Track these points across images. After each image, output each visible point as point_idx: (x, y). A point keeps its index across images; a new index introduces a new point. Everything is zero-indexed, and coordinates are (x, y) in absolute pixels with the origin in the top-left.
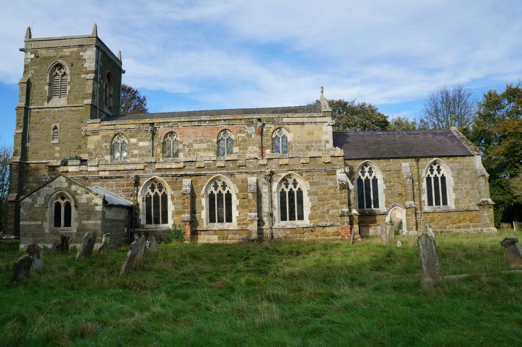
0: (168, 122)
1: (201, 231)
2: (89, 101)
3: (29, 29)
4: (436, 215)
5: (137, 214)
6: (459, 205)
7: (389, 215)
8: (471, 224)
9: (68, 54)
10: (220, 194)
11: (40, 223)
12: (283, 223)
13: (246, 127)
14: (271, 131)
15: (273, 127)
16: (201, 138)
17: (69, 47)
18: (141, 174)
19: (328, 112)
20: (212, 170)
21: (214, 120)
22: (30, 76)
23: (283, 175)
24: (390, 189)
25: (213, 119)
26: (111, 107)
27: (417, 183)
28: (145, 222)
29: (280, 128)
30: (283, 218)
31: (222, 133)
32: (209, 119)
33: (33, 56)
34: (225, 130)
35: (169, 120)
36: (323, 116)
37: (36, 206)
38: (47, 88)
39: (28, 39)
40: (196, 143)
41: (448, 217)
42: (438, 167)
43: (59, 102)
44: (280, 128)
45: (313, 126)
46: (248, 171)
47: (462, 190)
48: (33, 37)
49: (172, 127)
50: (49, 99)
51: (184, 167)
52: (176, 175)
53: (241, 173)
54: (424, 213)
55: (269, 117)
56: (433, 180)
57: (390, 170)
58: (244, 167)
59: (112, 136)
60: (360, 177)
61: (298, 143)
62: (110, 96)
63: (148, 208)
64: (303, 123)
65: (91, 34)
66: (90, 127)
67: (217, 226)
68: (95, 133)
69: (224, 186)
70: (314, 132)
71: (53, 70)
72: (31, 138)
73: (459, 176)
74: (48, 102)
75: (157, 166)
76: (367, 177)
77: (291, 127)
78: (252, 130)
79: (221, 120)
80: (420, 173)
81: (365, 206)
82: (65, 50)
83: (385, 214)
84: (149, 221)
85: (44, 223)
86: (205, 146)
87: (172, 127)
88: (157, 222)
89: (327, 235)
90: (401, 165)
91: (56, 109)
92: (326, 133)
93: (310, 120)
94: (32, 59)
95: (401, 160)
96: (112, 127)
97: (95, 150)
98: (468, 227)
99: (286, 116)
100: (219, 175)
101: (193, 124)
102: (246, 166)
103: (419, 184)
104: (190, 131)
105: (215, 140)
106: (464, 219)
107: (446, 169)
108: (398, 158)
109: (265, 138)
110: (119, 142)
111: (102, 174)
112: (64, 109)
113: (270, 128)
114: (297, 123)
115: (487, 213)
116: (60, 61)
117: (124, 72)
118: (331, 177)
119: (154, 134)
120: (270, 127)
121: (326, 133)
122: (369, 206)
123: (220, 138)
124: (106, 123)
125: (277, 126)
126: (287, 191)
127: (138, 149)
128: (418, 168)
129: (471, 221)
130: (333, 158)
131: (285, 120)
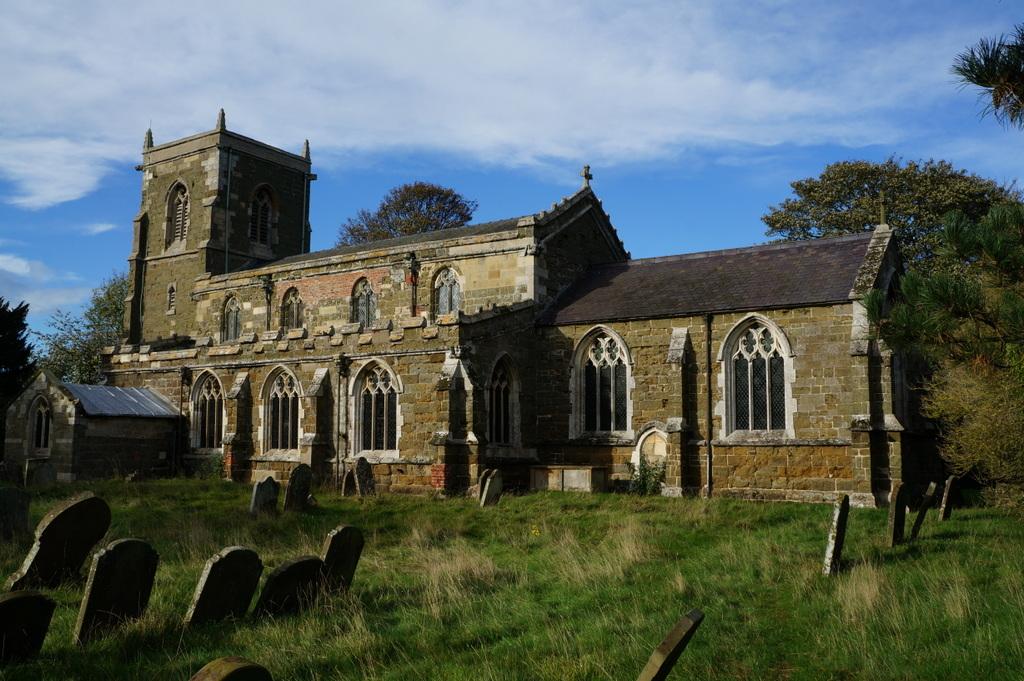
0: (289, 271)
1: (257, 461)
2: (204, 243)
3: (150, 134)
4: (746, 453)
5: (187, 431)
6: (805, 430)
7: (638, 447)
9: (189, 166)
11: (20, 441)
13: (392, 271)
14: (431, 275)
15: (434, 267)
16: (330, 296)
17: (188, 155)
19: (528, 226)
20: (273, 356)
21: (348, 262)
22: (147, 208)
23: (364, 363)
24: (644, 388)
25: (345, 259)
26: (275, 245)
27: (705, 375)
28: (199, 444)
29: (445, 268)
31: (360, 285)
32: (340, 260)
33: (151, 176)
34: (362, 279)
35: (289, 268)
36: (518, 237)
37: (19, 417)
38: (164, 225)
39: (146, 150)
40: (324, 306)
41: (776, 460)
43: (179, 246)
44: (445, 268)
45: (500, 258)
46: (316, 357)
47: (816, 390)
48: (157, 143)
49: (293, 279)
50: (168, 243)
51: (240, 352)
52: (229, 367)
54: (715, 446)
55: (427, 247)
57: (646, 344)
58: (312, 351)
59: (223, 299)
60: (590, 362)
61: (474, 296)
62: (274, 226)
64: (481, 255)
65: (215, 128)
66: (201, 286)
68: (204, 295)
69: (386, 379)
70: (502, 271)
71: (172, 196)
72: (146, 307)
74: (166, 248)
75: (212, 351)
76: (758, 353)
78: (400, 275)
79: (357, 261)
80: (712, 352)
81: (598, 425)
82: (186, 160)
83: (630, 445)
84: (203, 445)
85: (865, 417)
86: (333, 310)
87: (293, 279)
88: (211, 446)
91: (174, 259)
92: (523, 271)
93: (497, 246)
94: (150, 181)
95: (672, 321)
96: (223, 285)
97: (204, 324)
98: (828, 487)
99: (454, 243)
100: (280, 365)
102: (313, 348)
103: (709, 376)
104: (316, 283)
105: (348, 298)
107: (777, 337)
109: (420, 289)
110: (234, 309)
111: (156, 366)
112: (182, 258)
113: (429, 269)
114: (472, 256)
115: (861, 453)
116: (180, 180)
117: (314, 177)
118: (437, 366)
120: (428, 268)
121: (523, 271)
122: (606, 426)
123: (357, 294)
124: (217, 278)
125: (440, 265)
126: (373, 393)
127: (252, 320)
128: (709, 338)
130: (441, 328)
131: (453, 251)
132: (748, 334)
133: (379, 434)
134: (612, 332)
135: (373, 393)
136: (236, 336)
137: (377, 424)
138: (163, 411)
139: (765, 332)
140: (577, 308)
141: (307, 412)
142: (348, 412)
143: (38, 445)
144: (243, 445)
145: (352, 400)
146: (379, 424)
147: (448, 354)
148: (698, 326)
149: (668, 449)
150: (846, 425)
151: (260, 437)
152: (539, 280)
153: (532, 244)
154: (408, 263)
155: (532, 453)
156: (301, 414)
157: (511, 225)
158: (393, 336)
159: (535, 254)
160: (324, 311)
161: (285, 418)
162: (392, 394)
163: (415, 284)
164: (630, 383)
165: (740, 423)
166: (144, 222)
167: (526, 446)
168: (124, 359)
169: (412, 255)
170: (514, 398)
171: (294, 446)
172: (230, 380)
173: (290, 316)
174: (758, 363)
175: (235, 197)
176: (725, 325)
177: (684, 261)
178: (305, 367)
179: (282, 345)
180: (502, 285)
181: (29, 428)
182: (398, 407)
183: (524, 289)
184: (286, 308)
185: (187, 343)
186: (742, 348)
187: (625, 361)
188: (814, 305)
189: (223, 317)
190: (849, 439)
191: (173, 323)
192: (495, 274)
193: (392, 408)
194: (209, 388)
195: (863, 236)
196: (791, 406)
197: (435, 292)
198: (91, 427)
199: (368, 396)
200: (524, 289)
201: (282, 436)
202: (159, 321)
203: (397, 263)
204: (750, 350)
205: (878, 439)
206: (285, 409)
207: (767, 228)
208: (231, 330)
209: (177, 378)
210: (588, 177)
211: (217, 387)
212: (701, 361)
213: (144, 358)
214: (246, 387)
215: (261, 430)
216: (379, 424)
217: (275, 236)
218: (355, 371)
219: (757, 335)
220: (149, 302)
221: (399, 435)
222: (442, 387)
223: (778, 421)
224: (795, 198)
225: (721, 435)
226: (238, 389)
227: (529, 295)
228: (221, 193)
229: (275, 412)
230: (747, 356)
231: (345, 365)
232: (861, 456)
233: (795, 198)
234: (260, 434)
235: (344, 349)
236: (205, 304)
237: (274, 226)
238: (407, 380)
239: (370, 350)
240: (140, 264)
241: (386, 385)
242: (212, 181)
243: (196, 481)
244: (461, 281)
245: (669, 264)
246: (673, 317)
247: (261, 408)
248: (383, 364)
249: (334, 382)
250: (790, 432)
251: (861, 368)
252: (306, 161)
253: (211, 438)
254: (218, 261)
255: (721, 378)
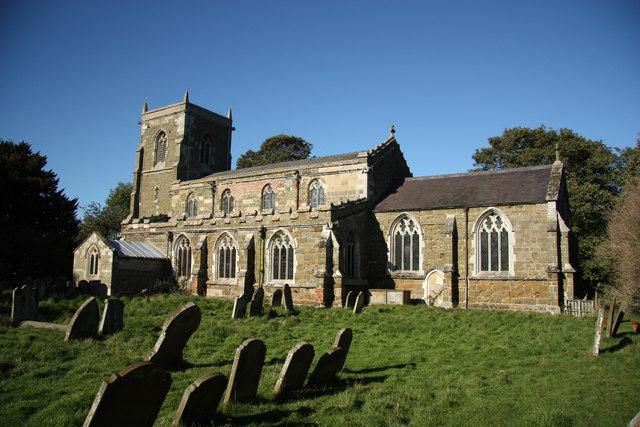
2: (176, 164)
4: (487, 283)
8: (537, 299)
10: (494, 233)
12: (274, 281)
17: (167, 116)
18: (174, 230)
23: (275, 231)
30: (276, 277)
42: (498, 218)
43: (161, 165)
45: (348, 174)
47: (527, 250)
50: (155, 164)
52: (196, 232)
53: (241, 229)
56: (411, 238)
62: (212, 155)
63: (398, 248)
64: (337, 172)
66: (175, 187)
67: (224, 280)
68: (177, 192)
69: (288, 241)
71: (159, 137)
73: (523, 229)
77: (326, 177)
78: (290, 183)
86: (251, 201)
89: (308, 296)
90: (445, 216)
101: (262, 178)
104: (241, 186)
105: (260, 195)
106: (528, 291)
107: (506, 220)
108: (443, 208)
110: (193, 200)
111: (152, 230)
114: (331, 173)
116: (163, 129)
117: (234, 129)
119: (214, 191)
120: (305, 180)
124: (184, 183)
126: (280, 248)
129: (537, 294)
131: (321, 170)
132: (402, 222)
133: (283, 271)
134: (411, 216)
135: (280, 248)
136: (195, 215)
137: (283, 262)
138: (159, 256)
139: (498, 218)
140: (391, 200)
141: (241, 258)
142: (267, 257)
143: (91, 273)
144: (203, 276)
145: (267, 252)
146: (283, 266)
147: (325, 227)
148: (459, 214)
149: (444, 281)
150: (543, 269)
151: (213, 271)
152: (370, 187)
153: (368, 168)
154: (295, 177)
155: (366, 282)
156: (237, 259)
157: (354, 156)
158: (292, 216)
159: (368, 173)
160: (245, 202)
161: (228, 261)
162: (291, 249)
163: (298, 189)
164: (422, 244)
165: (484, 267)
166: (142, 151)
167: (363, 278)
168: (135, 226)
169: (297, 172)
170: (357, 251)
171: (233, 276)
172: (196, 239)
173: (226, 204)
174: (407, 237)
175: (192, 139)
176: (476, 213)
177: (446, 180)
178: (240, 233)
179: (227, 220)
180: (350, 189)
181: (87, 263)
182: (295, 256)
183: (361, 192)
184: (223, 200)
185: (165, 218)
186: (485, 226)
187: (419, 233)
188: (525, 203)
189: (187, 205)
190: (546, 276)
191: (158, 207)
192: (345, 183)
193: (291, 256)
194: (183, 243)
195: (549, 166)
196: (512, 259)
197: (310, 193)
198: (121, 263)
199: (277, 250)
200: (361, 192)
201: (227, 270)
202: (148, 207)
203: (288, 176)
204: (489, 227)
205: (561, 277)
206: (185, 256)
207: (474, 162)
208: (192, 212)
209: (165, 237)
210: (393, 131)
211: (188, 243)
212: (461, 234)
213: (146, 226)
214: (205, 243)
215: (214, 267)
216: (283, 266)
217: (212, 161)
218: (269, 235)
219: (493, 219)
220: (143, 195)
221: (295, 271)
222: (321, 245)
223: (505, 267)
224: (489, 146)
225: (474, 274)
226: (201, 244)
227: (364, 195)
228: (185, 136)
229: (222, 255)
230: (488, 231)
231: (263, 232)
232: (553, 286)
233: (489, 146)
234: (213, 269)
235: (263, 223)
236: (176, 198)
237: (212, 155)
238: (300, 241)
239: (278, 224)
240: (139, 174)
241: (287, 243)
242: (181, 130)
243: (173, 297)
244: (325, 186)
245: (440, 180)
246: (446, 208)
247: (214, 255)
248: (286, 232)
249: (256, 241)
250: (512, 272)
251: (553, 237)
252: (230, 120)
253: (184, 267)
254: (185, 173)
255: (475, 243)
